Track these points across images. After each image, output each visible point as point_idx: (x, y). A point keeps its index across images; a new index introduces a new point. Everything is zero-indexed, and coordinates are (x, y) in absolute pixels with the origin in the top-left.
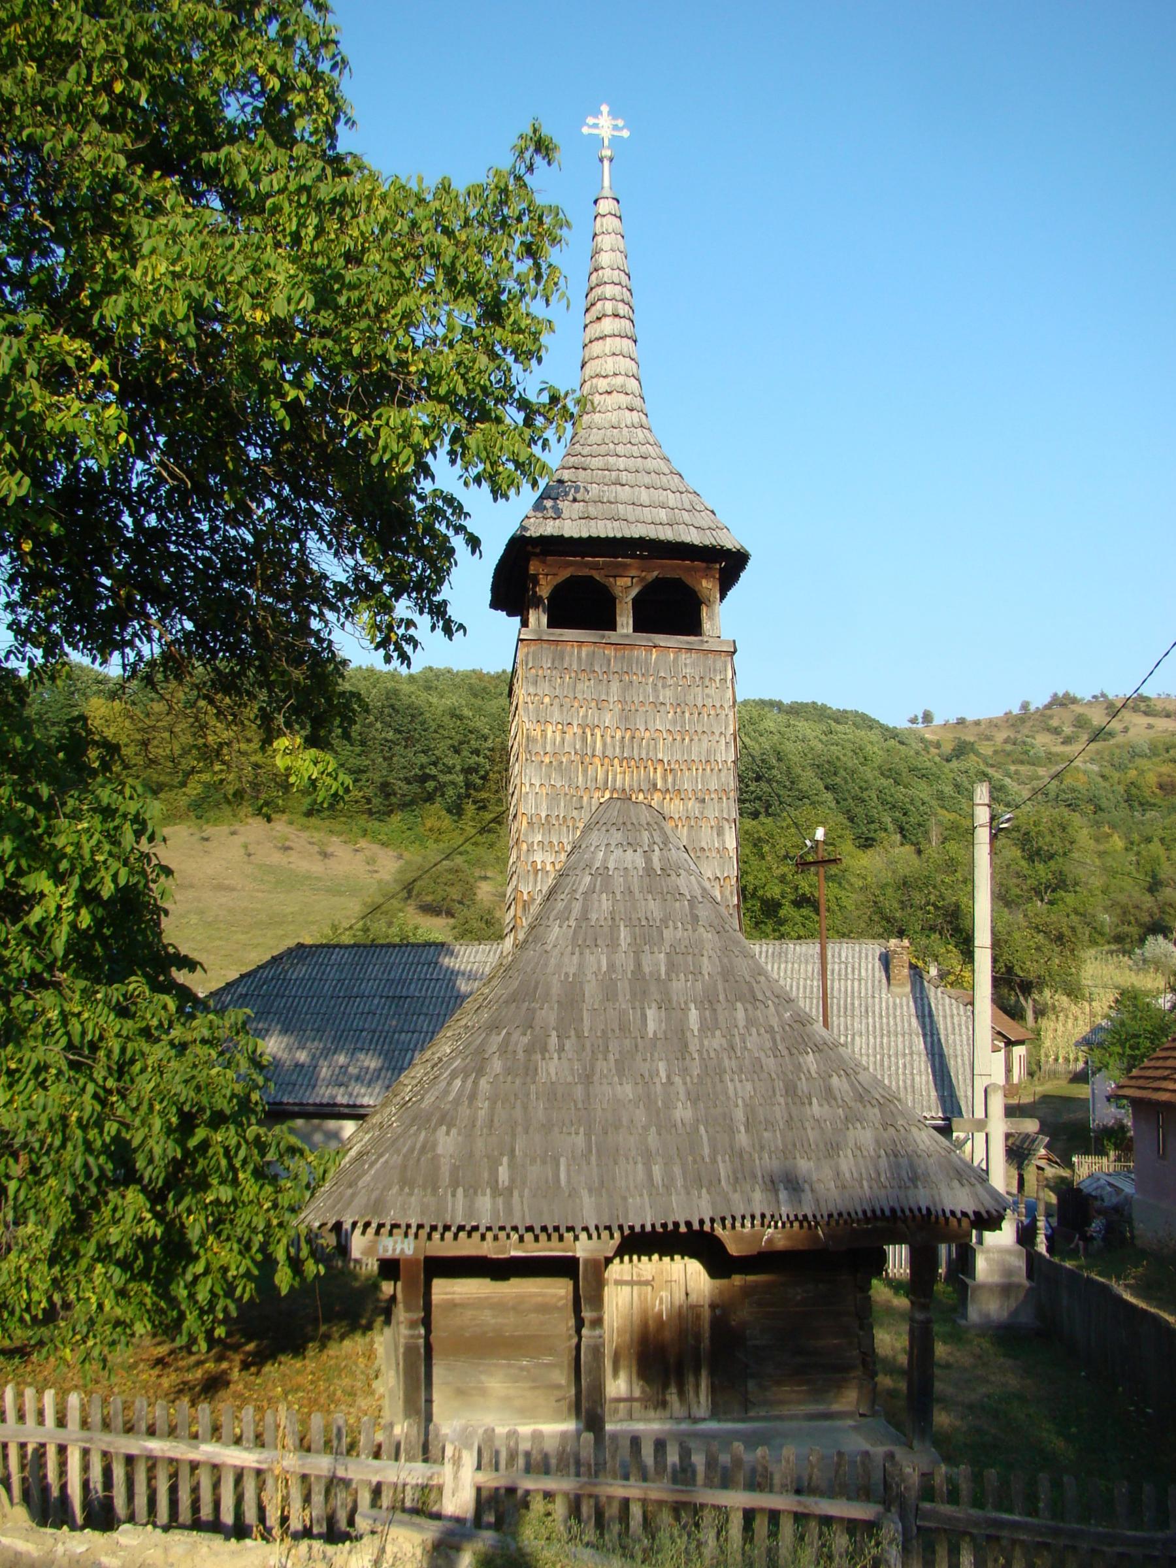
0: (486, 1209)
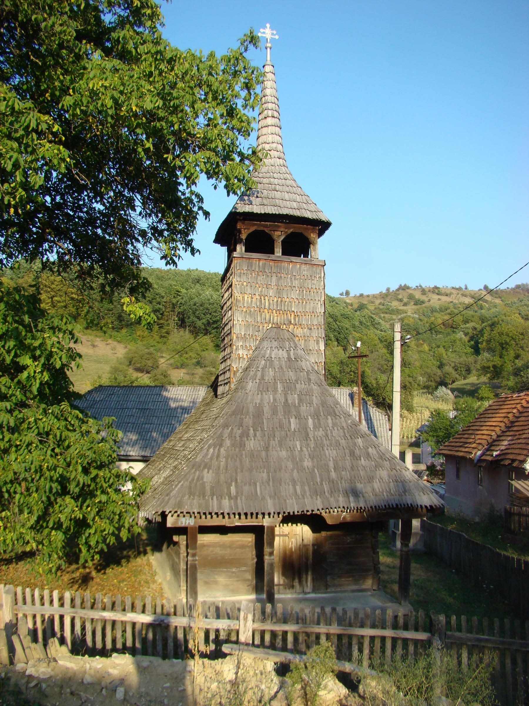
0: (226, 505)
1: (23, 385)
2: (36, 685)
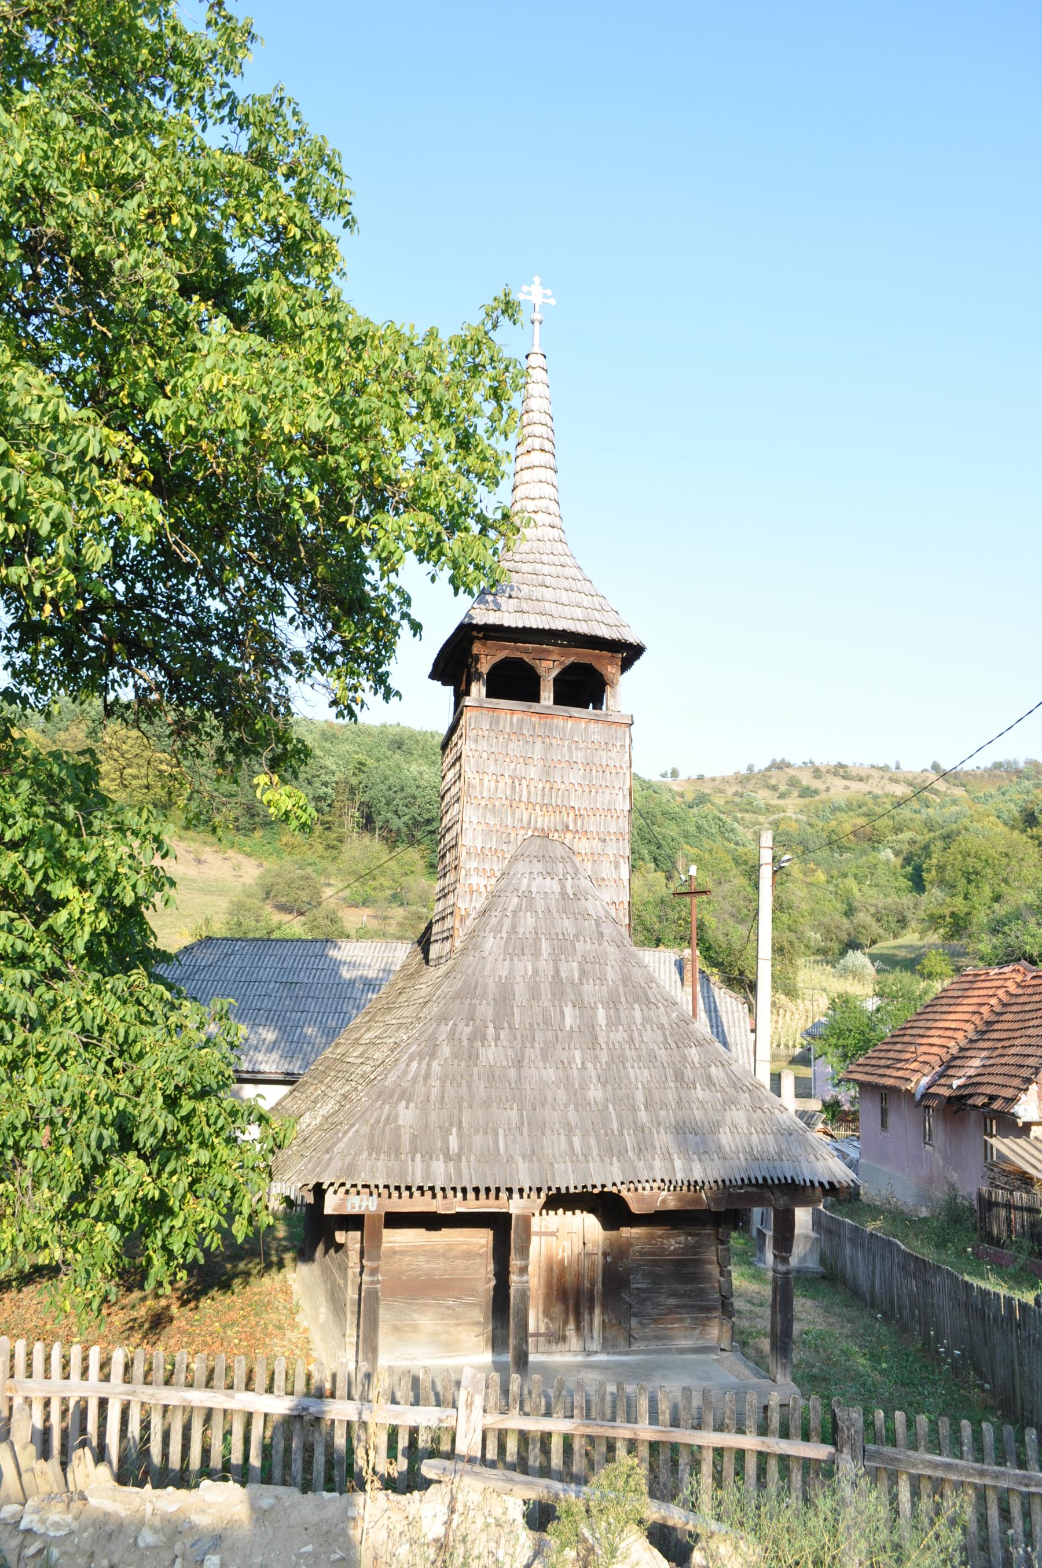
0: (440, 1174)
1: (58, 936)
2: (40, 1552)
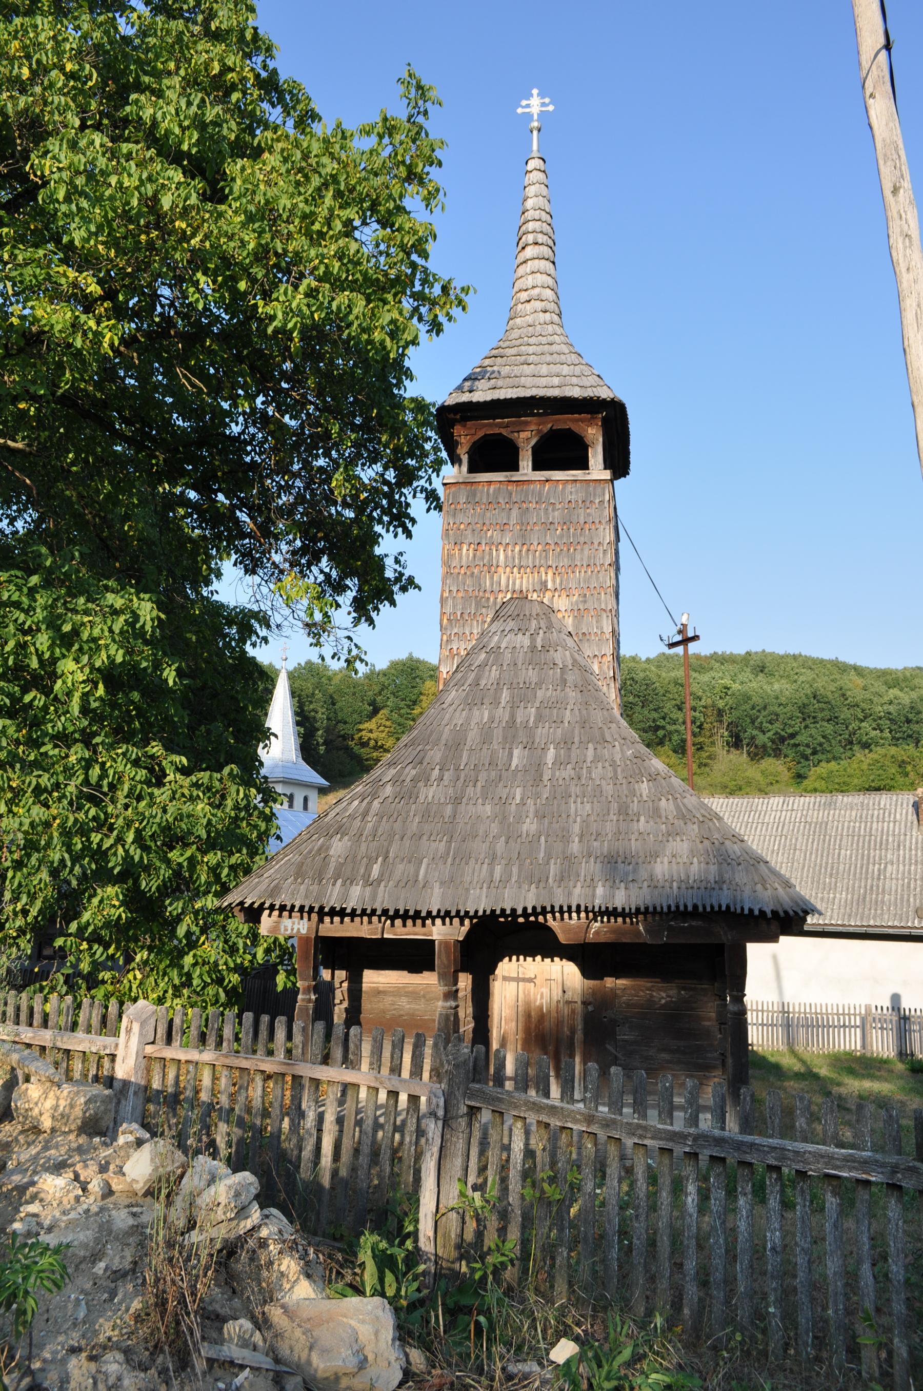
0: (355, 898)
